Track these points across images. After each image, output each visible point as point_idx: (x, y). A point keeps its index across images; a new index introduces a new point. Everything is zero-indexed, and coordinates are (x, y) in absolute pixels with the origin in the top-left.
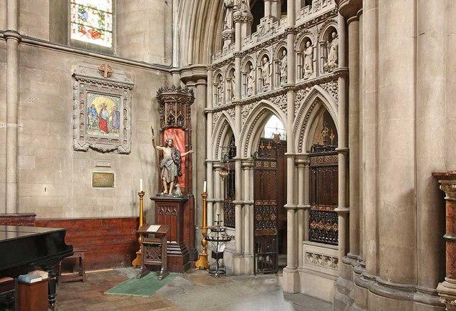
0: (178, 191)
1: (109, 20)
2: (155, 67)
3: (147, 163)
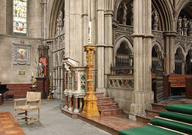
0: (43, 76)
1: (25, 25)
2: (38, 39)
3: (36, 68)
